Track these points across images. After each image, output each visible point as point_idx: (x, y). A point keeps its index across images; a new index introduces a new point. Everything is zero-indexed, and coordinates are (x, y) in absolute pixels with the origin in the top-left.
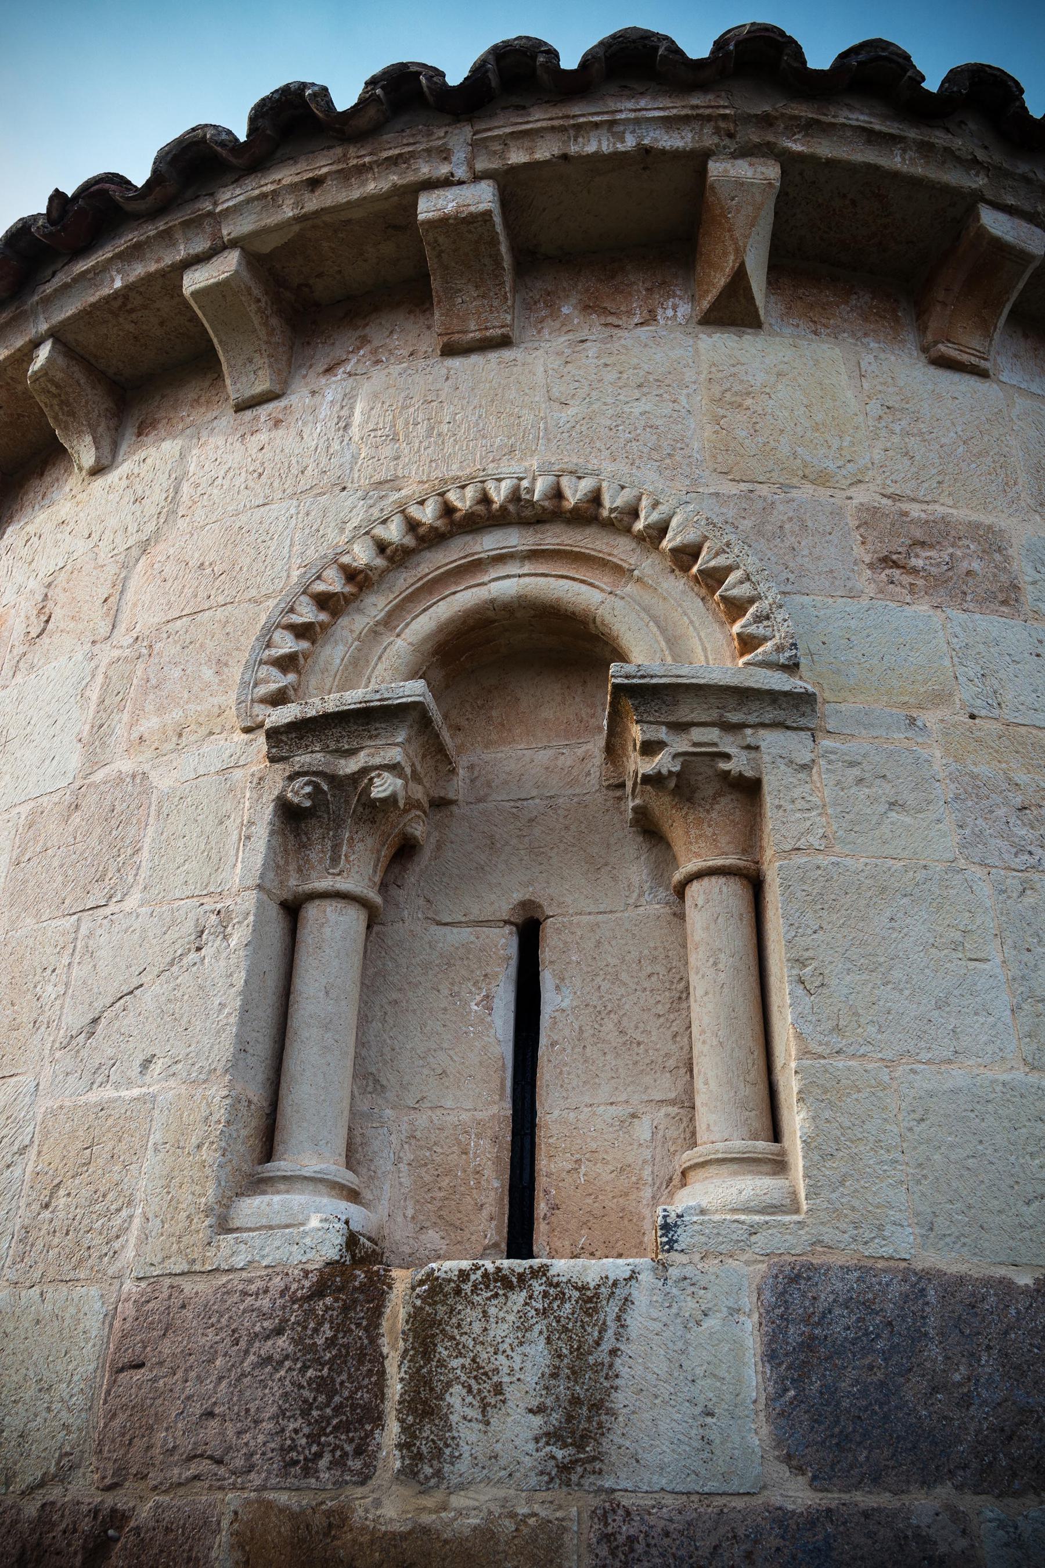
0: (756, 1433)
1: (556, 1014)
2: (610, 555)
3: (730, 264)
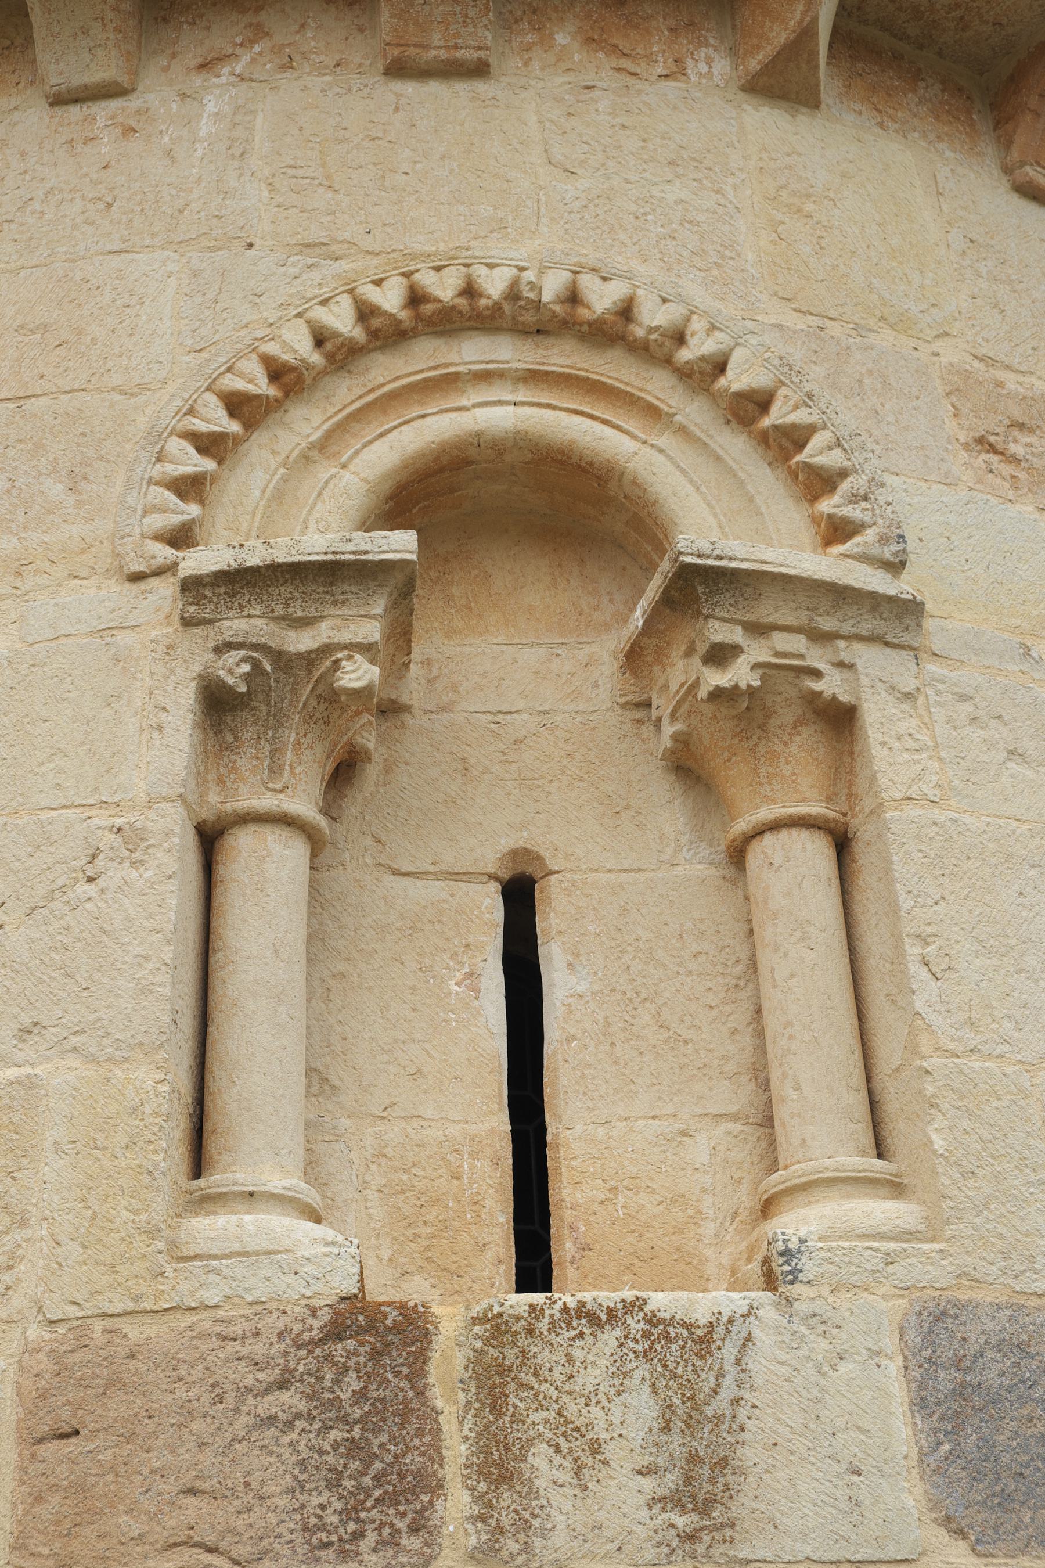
0: (910, 1492)
1: (570, 1000)
2: (641, 390)
3: (797, 14)
